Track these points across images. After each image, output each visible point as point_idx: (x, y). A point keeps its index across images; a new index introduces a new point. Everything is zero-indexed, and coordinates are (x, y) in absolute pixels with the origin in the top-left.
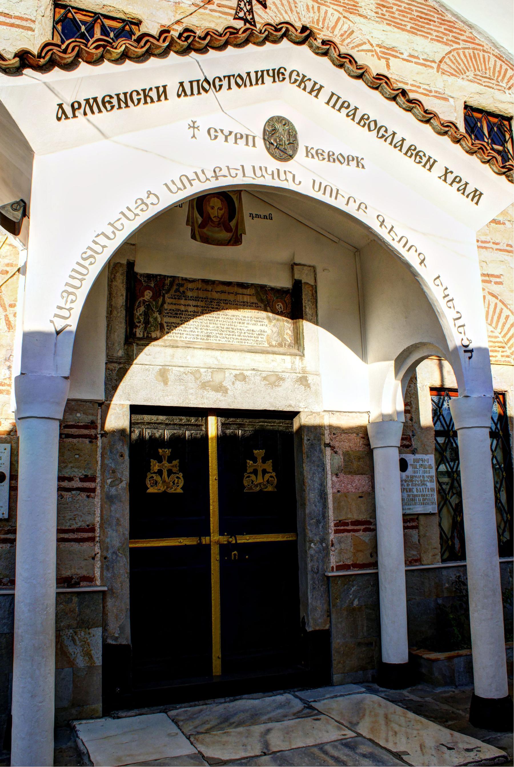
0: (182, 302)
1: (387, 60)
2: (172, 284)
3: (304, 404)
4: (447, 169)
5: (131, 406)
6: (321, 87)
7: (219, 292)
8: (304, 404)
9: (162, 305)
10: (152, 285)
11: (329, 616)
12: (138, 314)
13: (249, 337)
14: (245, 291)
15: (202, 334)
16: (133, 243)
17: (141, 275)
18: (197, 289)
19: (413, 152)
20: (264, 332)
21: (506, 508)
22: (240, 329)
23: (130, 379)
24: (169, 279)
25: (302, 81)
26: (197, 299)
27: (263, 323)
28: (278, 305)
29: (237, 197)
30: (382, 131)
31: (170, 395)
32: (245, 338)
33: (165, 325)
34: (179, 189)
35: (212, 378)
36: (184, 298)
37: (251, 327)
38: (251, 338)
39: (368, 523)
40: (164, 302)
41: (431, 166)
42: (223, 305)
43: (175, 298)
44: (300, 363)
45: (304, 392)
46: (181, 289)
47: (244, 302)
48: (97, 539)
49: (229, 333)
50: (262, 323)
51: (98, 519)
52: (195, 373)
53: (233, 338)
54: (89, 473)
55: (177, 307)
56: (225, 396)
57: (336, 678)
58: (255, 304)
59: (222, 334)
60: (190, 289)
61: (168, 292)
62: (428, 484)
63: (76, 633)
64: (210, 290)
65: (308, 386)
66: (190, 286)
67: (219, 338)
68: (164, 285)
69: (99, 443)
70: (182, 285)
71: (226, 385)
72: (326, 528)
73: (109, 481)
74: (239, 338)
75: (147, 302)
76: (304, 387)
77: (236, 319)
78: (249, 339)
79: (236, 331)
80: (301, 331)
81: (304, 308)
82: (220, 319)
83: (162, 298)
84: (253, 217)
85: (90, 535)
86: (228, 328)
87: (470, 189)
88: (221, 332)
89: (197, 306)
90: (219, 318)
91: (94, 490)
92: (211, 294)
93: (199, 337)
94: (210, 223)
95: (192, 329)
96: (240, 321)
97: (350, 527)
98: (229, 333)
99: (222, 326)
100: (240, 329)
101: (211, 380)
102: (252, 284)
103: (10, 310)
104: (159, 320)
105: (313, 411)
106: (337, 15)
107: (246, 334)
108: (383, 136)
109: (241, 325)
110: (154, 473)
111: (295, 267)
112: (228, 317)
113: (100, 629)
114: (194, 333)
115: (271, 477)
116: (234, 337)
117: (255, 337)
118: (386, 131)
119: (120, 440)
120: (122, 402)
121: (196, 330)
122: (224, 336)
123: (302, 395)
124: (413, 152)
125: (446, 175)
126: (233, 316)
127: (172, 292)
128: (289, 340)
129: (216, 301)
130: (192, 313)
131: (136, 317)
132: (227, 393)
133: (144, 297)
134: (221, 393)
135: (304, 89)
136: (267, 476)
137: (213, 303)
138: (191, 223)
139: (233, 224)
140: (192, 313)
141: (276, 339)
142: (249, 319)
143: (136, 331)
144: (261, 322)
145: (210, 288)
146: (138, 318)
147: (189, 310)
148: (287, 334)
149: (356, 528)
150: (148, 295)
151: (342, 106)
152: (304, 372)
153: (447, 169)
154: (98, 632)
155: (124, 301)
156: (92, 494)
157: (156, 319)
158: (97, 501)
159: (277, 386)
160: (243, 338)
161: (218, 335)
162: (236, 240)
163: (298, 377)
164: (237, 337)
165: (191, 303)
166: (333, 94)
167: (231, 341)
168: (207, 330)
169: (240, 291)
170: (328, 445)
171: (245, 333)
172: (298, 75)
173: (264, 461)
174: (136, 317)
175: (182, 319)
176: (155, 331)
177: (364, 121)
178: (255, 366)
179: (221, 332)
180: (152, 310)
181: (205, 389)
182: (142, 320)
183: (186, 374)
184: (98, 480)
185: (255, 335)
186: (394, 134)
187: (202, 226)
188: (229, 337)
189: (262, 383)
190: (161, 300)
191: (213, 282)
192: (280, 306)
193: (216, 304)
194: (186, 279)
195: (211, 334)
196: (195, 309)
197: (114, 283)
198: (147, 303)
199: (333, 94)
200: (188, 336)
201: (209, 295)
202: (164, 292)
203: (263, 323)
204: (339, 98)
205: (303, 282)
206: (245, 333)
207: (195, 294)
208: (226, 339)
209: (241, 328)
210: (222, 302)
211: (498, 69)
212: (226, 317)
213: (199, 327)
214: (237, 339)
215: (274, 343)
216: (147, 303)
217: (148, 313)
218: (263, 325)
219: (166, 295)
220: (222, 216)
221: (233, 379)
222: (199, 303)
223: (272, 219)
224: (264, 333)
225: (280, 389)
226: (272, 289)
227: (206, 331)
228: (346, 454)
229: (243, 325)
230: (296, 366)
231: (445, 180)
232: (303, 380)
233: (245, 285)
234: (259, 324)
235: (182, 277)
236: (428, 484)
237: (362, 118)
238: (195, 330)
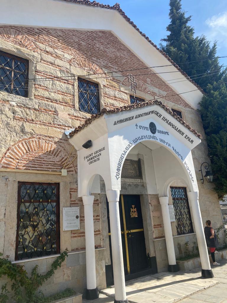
1: (154, 96)
4: (186, 135)
5: (18, 182)
6: (161, 115)
11: (155, 252)
19: (180, 131)
21: (56, 212)
25: (157, 114)
30: (173, 126)
34: (136, 142)
37: (130, 171)
39: (160, 225)
41: (183, 134)
48: (101, 234)
51: (101, 228)
54: (98, 215)
57: (159, 271)
62: (173, 213)
63: (99, 262)
65: (144, 187)
69: (100, 205)
72: (152, 227)
73: (103, 216)
85: (99, 232)
87: (191, 140)
91: (99, 219)
97: (157, 226)
103: (76, 167)
106: (142, 83)
108: (173, 127)
111: (139, 155)
113: (104, 261)
118: (174, 126)
124: (180, 131)
125: (186, 137)
135: (158, 116)
149: (158, 226)
151: (165, 120)
153: (186, 135)
154: (104, 261)
156: (99, 220)
158: (153, 224)
166: (164, 117)
170: (150, 203)
172: (157, 112)
177: (170, 124)
184: (100, 216)
186: (176, 127)
199: (164, 117)
204: (165, 118)
211: (178, 98)
221: (128, 185)
226: (134, 161)
228: (154, 205)
231: (186, 138)
232: (143, 186)
236: (173, 213)
237: (169, 123)
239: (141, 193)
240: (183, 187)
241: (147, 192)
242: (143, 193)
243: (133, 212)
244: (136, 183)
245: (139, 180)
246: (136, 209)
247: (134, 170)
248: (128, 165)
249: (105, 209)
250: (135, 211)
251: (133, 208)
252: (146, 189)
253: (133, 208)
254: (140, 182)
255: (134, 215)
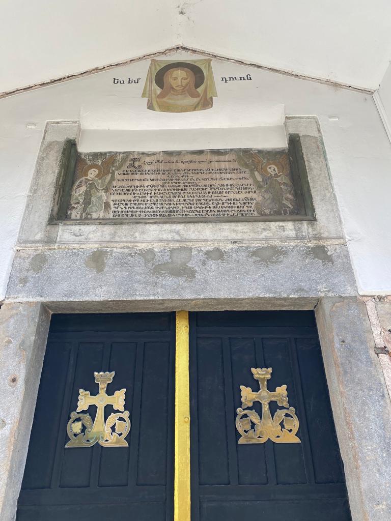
0: (137, 177)
2: (124, 160)
3: (324, 285)
7: (186, 162)
8: (324, 285)
9: (110, 182)
10: (99, 163)
12: (77, 194)
13: (229, 207)
14: (222, 158)
15: (162, 210)
16: (75, 120)
17: (86, 155)
18: (158, 162)
20: (252, 199)
22: (216, 200)
23: (48, 268)
24: (121, 155)
26: (157, 172)
27: (250, 190)
28: (270, 168)
29: (205, 67)
31: (105, 285)
32: (224, 209)
33: (112, 203)
35: (171, 258)
36: (139, 173)
37: (232, 196)
38: (233, 209)
40: (113, 179)
42: (192, 175)
43: (128, 174)
44: (310, 230)
45: (322, 268)
46: (137, 164)
47: (220, 170)
49: (200, 206)
50: (247, 190)
52: (148, 255)
53: (207, 211)
55: (130, 183)
56: (191, 282)
58: (237, 170)
59: (191, 208)
60: (148, 163)
61: (118, 168)
64: (175, 162)
66: (148, 159)
67: (186, 213)
68: (114, 162)
70: (139, 160)
71: (193, 266)
74: (215, 209)
75: (89, 180)
76: (321, 261)
77: (211, 189)
78: (230, 209)
79: (210, 203)
80: (306, 189)
81: (306, 163)
82: (188, 191)
83: (110, 175)
84: (226, 80)
86: (199, 200)
88: (190, 206)
89: (156, 180)
90: (186, 190)
92: (176, 165)
93: (158, 214)
94: (172, 92)
95: (148, 205)
96: (217, 190)
98: (200, 206)
99: (191, 198)
100: (216, 200)
101: (170, 261)
102: (232, 150)
104: (104, 199)
105: (343, 295)
107: (226, 205)
109: (217, 195)
110: (248, 408)
112: (198, 187)
114: (152, 210)
115: (121, 419)
116: (208, 209)
117: (238, 207)
119: (16, 354)
120: (31, 299)
121: (154, 207)
122: (193, 209)
123: (319, 273)
126: (206, 186)
127: (125, 168)
128: (290, 206)
129: (182, 172)
130: (149, 188)
131: (74, 198)
132: (194, 277)
133: (87, 175)
134: (184, 279)
136: (113, 418)
137: (178, 175)
138: (147, 95)
139: (200, 90)
140: (149, 188)
141: (270, 206)
142: (229, 187)
143: (71, 213)
144: (246, 188)
145: (174, 159)
146: (77, 199)
147: (146, 185)
148: (287, 199)
150: (92, 174)
152: (318, 238)
155: (55, 178)
157: (100, 198)
159: (276, 262)
160: (221, 209)
161: (184, 209)
162: (206, 103)
163: (308, 247)
164: (212, 209)
165: (148, 177)
167: (204, 214)
168: (170, 204)
169: (216, 158)
171: (223, 203)
173: (271, 387)
174: (74, 198)
175: (136, 195)
176: (97, 211)
178: (234, 236)
179: (190, 206)
180: (97, 189)
181: (161, 274)
182: (81, 201)
183: (132, 256)
185: (239, 205)
187: (161, 96)
188: (201, 210)
189: (250, 260)
190: (109, 177)
191: (179, 153)
192: (272, 169)
193: (182, 175)
194: (143, 153)
195: (175, 209)
196: (154, 183)
197: (46, 161)
198: (90, 182)
200: (142, 214)
201: (173, 166)
202: (113, 169)
203: (250, 190)
205: (301, 135)
206: (223, 203)
207: (154, 167)
208: (196, 213)
209: (218, 198)
210: (190, 172)
212: (197, 188)
213: (159, 202)
214: (212, 211)
215: (267, 211)
216: (90, 182)
217: (90, 192)
218: (249, 192)
219: (116, 172)
220: (187, 85)
221: (203, 258)
222: (159, 177)
223: (251, 79)
224: (252, 202)
225: (280, 266)
227: (167, 206)
229: (220, 195)
230: (304, 234)
232: (319, 253)
233: (223, 151)
234: (244, 191)
235: (138, 152)
238: (153, 205)
239: (301, 290)
240: (238, 223)
241: (353, 282)
242: (321, 290)
243: (92, 410)
244: (267, 239)
245: (289, 225)
246: (282, 390)
247: (260, 187)
248: (225, 171)
249: (14, 380)
250: (109, 410)
251: (103, 387)
252: (348, 269)
253: (103, 387)
254: (292, 234)
255: (280, 429)
